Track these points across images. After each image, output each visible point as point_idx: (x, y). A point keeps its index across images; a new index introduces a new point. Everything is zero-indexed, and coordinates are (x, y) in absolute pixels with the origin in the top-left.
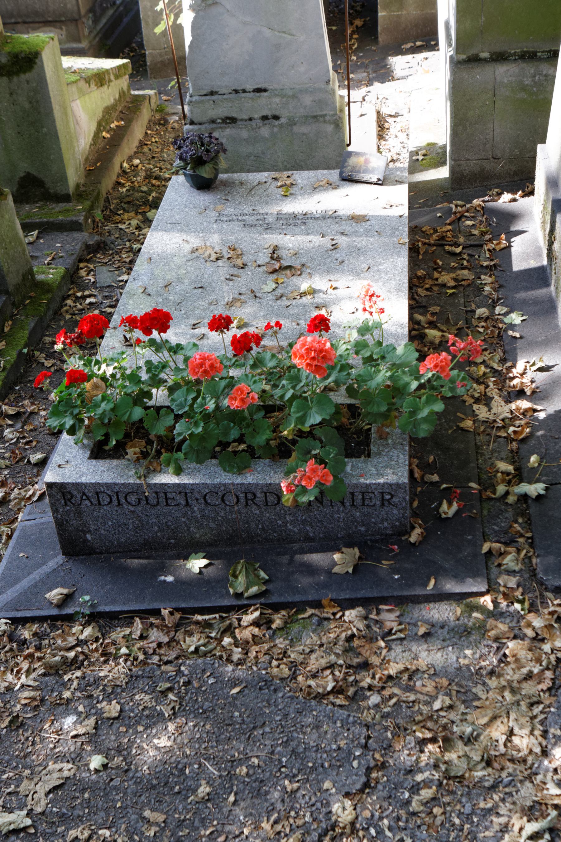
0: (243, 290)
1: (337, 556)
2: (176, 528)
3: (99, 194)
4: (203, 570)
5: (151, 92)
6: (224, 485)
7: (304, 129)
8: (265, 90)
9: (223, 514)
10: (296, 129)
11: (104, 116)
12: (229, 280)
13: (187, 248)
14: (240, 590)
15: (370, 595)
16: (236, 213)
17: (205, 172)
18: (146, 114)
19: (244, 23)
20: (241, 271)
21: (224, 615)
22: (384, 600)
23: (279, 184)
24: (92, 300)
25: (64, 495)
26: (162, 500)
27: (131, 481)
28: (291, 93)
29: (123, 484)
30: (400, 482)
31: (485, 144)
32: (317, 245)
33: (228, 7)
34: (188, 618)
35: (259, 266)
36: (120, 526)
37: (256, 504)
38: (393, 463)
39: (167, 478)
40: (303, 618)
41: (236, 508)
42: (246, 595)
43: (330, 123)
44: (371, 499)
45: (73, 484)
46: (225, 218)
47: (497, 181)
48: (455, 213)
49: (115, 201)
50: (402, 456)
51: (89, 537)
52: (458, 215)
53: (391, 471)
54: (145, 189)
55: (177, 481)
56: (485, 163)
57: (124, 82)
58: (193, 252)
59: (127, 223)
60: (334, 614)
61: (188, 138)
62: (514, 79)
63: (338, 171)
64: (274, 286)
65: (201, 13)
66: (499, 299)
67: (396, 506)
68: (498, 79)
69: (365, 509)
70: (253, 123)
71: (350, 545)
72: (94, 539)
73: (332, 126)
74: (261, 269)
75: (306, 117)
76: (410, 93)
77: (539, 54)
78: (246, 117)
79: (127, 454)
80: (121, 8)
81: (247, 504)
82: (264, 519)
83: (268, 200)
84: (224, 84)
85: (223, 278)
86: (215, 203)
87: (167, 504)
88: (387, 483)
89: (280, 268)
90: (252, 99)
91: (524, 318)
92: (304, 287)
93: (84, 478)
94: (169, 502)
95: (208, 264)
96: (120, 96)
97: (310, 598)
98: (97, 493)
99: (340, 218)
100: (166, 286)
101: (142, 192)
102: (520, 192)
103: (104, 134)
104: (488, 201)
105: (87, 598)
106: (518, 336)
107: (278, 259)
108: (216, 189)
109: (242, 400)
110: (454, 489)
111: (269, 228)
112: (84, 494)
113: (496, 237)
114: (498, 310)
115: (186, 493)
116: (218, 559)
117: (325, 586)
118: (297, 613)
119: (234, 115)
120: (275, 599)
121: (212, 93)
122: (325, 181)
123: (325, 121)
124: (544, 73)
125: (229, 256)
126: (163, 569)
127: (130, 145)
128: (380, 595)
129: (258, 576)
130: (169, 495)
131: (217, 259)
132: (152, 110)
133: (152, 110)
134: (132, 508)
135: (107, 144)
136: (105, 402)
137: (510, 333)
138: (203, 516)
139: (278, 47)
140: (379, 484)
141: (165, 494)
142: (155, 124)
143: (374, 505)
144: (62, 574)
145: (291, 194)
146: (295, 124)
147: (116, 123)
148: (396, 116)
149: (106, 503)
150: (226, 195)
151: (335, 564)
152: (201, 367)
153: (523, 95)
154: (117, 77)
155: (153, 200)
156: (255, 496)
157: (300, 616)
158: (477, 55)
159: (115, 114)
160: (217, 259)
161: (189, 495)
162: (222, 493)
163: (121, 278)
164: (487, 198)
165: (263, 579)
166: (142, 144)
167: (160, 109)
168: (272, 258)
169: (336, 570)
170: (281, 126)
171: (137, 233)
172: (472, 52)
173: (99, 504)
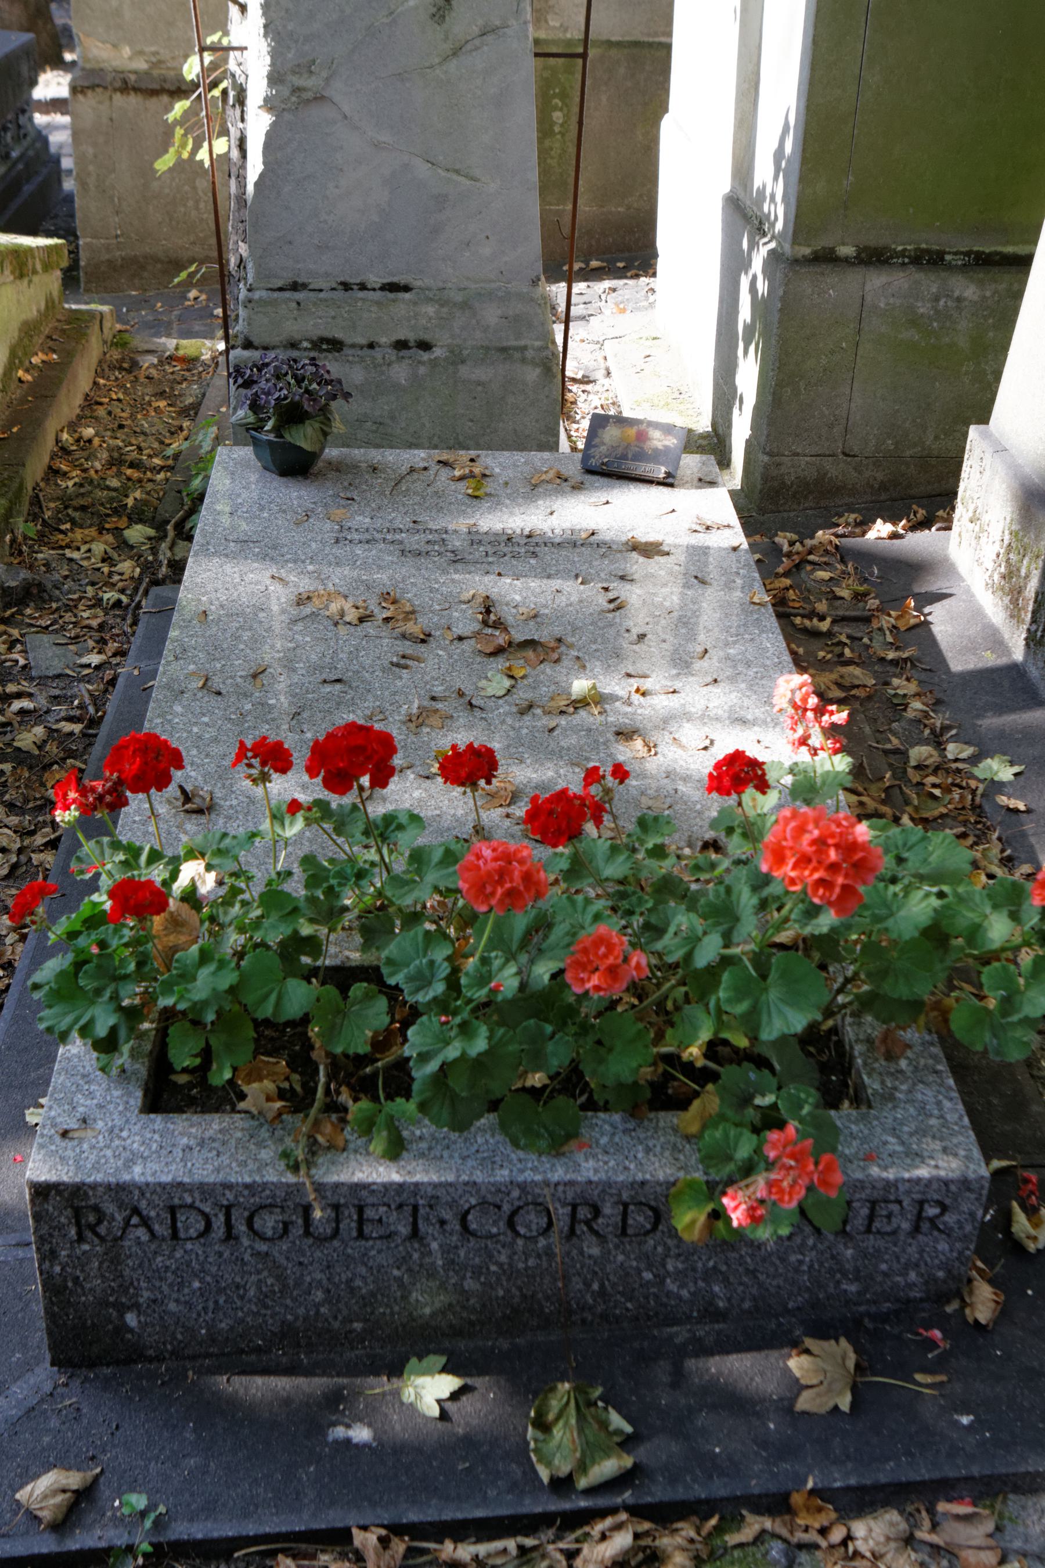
0: (439, 690)
1: (796, 1364)
2: (373, 1294)
3: (21, 487)
4: (448, 1405)
5: (105, 308)
6: (523, 1187)
7: (481, 373)
8: (406, 289)
9: (503, 1258)
10: (464, 371)
11: (21, 339)
12: (398, 665)
14: (564, 1468)
15: (914, 1476)
17: (303, 437)
18: (94, 349)
19: (377, 146)
20: (422, 648)
21: (529, 1542)
22: (945, 1488)
23: (457, 473)
24: (26, 704)
25: (77, 1213)
26: (349, 1225)
27: (271, 1176)
28: (459, 298)
29: (247, 1186)
30: (971, 1176)
31: (831, 426)
32: (574, 598)
33: (346, 108)
34: (426, 1551)
35: (460, 639)
36: (221, 1291)
37: (596, 1233)
38: (933, 1122)
39: (372, 1170)
40: (741, 1545)
41: (542, 1242)
42: (583, 1483)
43: (534, 363)
44: (889, 1216)
45: (109, 1187)
47: (847, 500)
48: (789, 555)
49: (52, 505)
50: (947, 1104)
51: (131, 1319)
52: (797, 559)
53: (937, 1145)
55: (396, 1178)
56: (828, 464)
57: (53, 281)
59: (84, 548)
60: (823, 1531)
62: (898, 302)
64: (507, 683)
65: (287, 116)
66: (945, 728)
67: (947, 1232)
68: (868, 299)
69: (871, 1241)
70: (378, 353)
71: (824, 1331)
72: (143, 1326)
73: (538, 371)
74: (466, 645)
75: (487, 349)
76: (601, 344)
77: (948, 257)
78: (363, 341)
79: (242, 1097)
80: (20, 166)
81: (572, 1231)
82: (609, 1268)
83: (440, 503)
84: (323, 269)
85: (386, 663)
87: (361, 1235)
88: (939, 1179)
89: (510, 644)
90: (378, 303)
91: (1017, 769)
92: (580, 686)
93: (137, 1169)
94: (367, 1229)
97: (755, 1486)
98: (173, 1210)
100: (255, 676)
101: (108, 488)
102: (904, 522)
103: (20, 373)
104: (843, 536)
105: (139, 1501)
106: (1022, 807)
107: (499, 625)
108: (320, 475)
109: (613, 972)
110: (1020, 1172)
111: (457, 560)
112: (136, 1211)
113: (898, 602)
114: (952, 750)
115: (415, 1208)
116: (481, 1373)
117: (782, 1450)
118: (719, 1530)
119: (339, 335)
120: (658, 1493)
121: (295, 287)
122: (551, 475)
123: (523, 360)
124: (957, 294)
125: (388, 614)
126: (335, 1404)
127: (69, 404)
128: (936, 1475)
129: (604, 1424)
130: (370, 1213)
131: (361, 620)
132: (105, 342)
134: (263, 1247)
135: (27, 394)
136: (212, 967)
137: (1003, 800)
138: (450, 1263)
139: (441, 200)
140: (918, 1180)
141: (360, 1210)
142: (112, 368)
143: (894, 1233)
144: (54, 1423)
145: (487, 495)
146: (463, 362)
148: (586, 380)
149: (192, 1232)
151: (798, 1387)
152: (500, 882)
153: (911, 334)
154: (47, 267)
155: (134, 507)
156: (597, 1212)
157: (732, 1539)
158: (832, 250)
159: (39, 340)
160: (361, 620)
161: (422, 1211)
162: (515, 1208)
163: (85, 660)
164: (840, 530)
165: (619, 1432)
166: (90, 403)
167: (119, 341)
168: (485, 623)
169: (804, 1402)
170: (434, 363)
171: (106, 570)
172: (823, 242)
173: (175, 1235)
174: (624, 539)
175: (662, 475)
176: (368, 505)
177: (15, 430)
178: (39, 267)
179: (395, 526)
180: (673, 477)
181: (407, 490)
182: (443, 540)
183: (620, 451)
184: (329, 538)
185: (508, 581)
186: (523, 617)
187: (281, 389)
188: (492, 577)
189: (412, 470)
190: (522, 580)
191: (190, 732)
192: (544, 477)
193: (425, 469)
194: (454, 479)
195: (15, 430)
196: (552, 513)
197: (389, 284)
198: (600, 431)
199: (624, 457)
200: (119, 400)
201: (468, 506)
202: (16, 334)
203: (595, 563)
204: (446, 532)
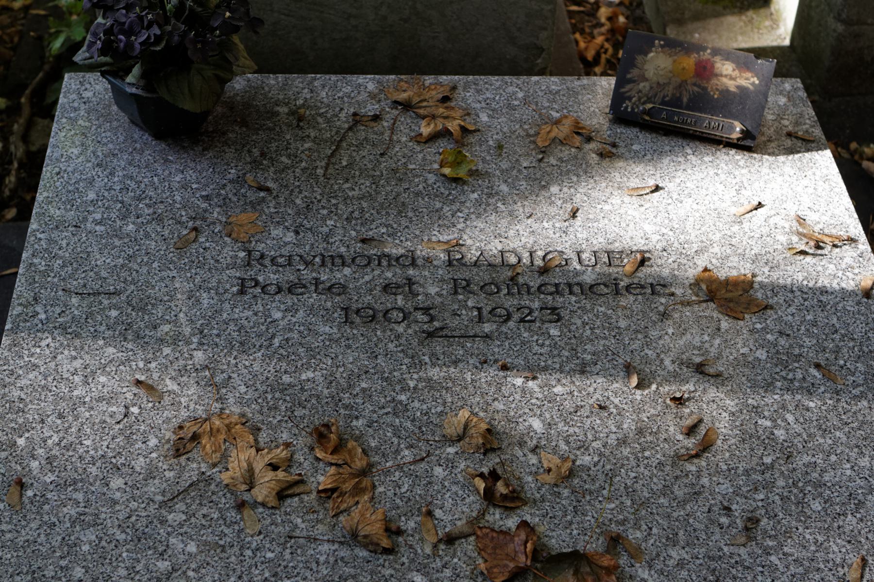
13: (161, 424)
35: (450, 540)
58: (183, 445)
63: (606, 84)
86: (225, 203)
95: (251, 521)
99: (658, 287)
131: (282, 495)
150: (256, 164)
168: (489, 496)
174: (692, 273)
175: (735, 135)
180: (753, 138)
181: (350, 165)
182: (410, 282)
183: (669, 91)
185: (519, 381)
186: (549, 478)
188: (492, 372)
189: (357, 119)
190: (542, 377)
192: (555, 132)
193: (376, 118)
194: (418, 139)
196: (574, 214)
198: (639, 58)
199: (676, 102)
201: (448, 201)
204: (413, 264)
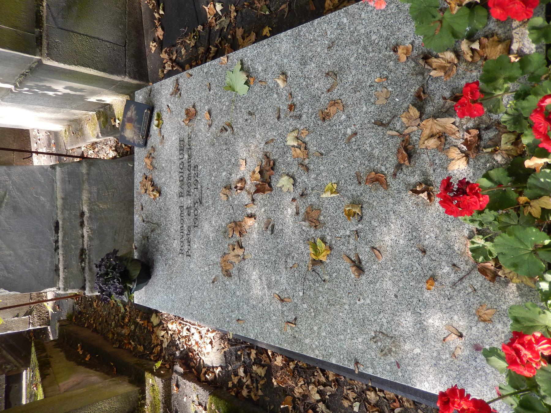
16: (179, 237)
46: (186, 247)
54: (133, 327)
61: (100, 288)
73: (92, 168)
96: (59, 347)
101: (135, 329)
133: (70, 323)
147: (79, 350)
176: (167, 241)
177: (112, 364)
178: (44, 354)
179: (179, 229)
184: (187, 259)
187: (114, 282)
191: (325, 337)
195: (112, 364)
197: (55, 231)
200: (94, 320)
202: (72, 362)
203: (201, 138)
